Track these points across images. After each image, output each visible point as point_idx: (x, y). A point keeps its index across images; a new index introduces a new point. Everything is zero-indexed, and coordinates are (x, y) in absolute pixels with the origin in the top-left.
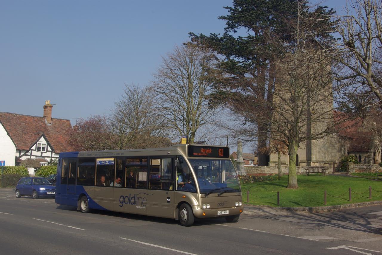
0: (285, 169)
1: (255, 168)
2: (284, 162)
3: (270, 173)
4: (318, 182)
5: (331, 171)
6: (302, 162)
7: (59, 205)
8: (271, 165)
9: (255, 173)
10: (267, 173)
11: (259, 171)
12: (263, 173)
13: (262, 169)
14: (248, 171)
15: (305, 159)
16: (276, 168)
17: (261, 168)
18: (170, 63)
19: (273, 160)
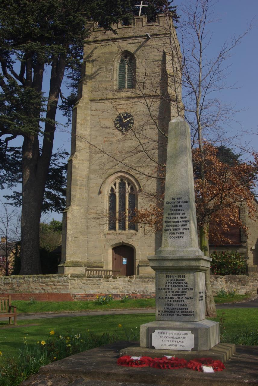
0: (129, 281)
1: (36, 279)
2: (99, 265)
3: (82, 292)
4: (191, 315)
5: (253, 289)
6: (144, 264)
7: (19, 75)
8: (69, 271)
9: (37, 292)
10: (75, 292)
11: (49, 288)
12: (63, 292)
13: (59, 282)
14: (15, 286)
15: (164, 255)
16: (102, 279)
17: (56, 280)
18: (10, 28)
19: (72, 259)
